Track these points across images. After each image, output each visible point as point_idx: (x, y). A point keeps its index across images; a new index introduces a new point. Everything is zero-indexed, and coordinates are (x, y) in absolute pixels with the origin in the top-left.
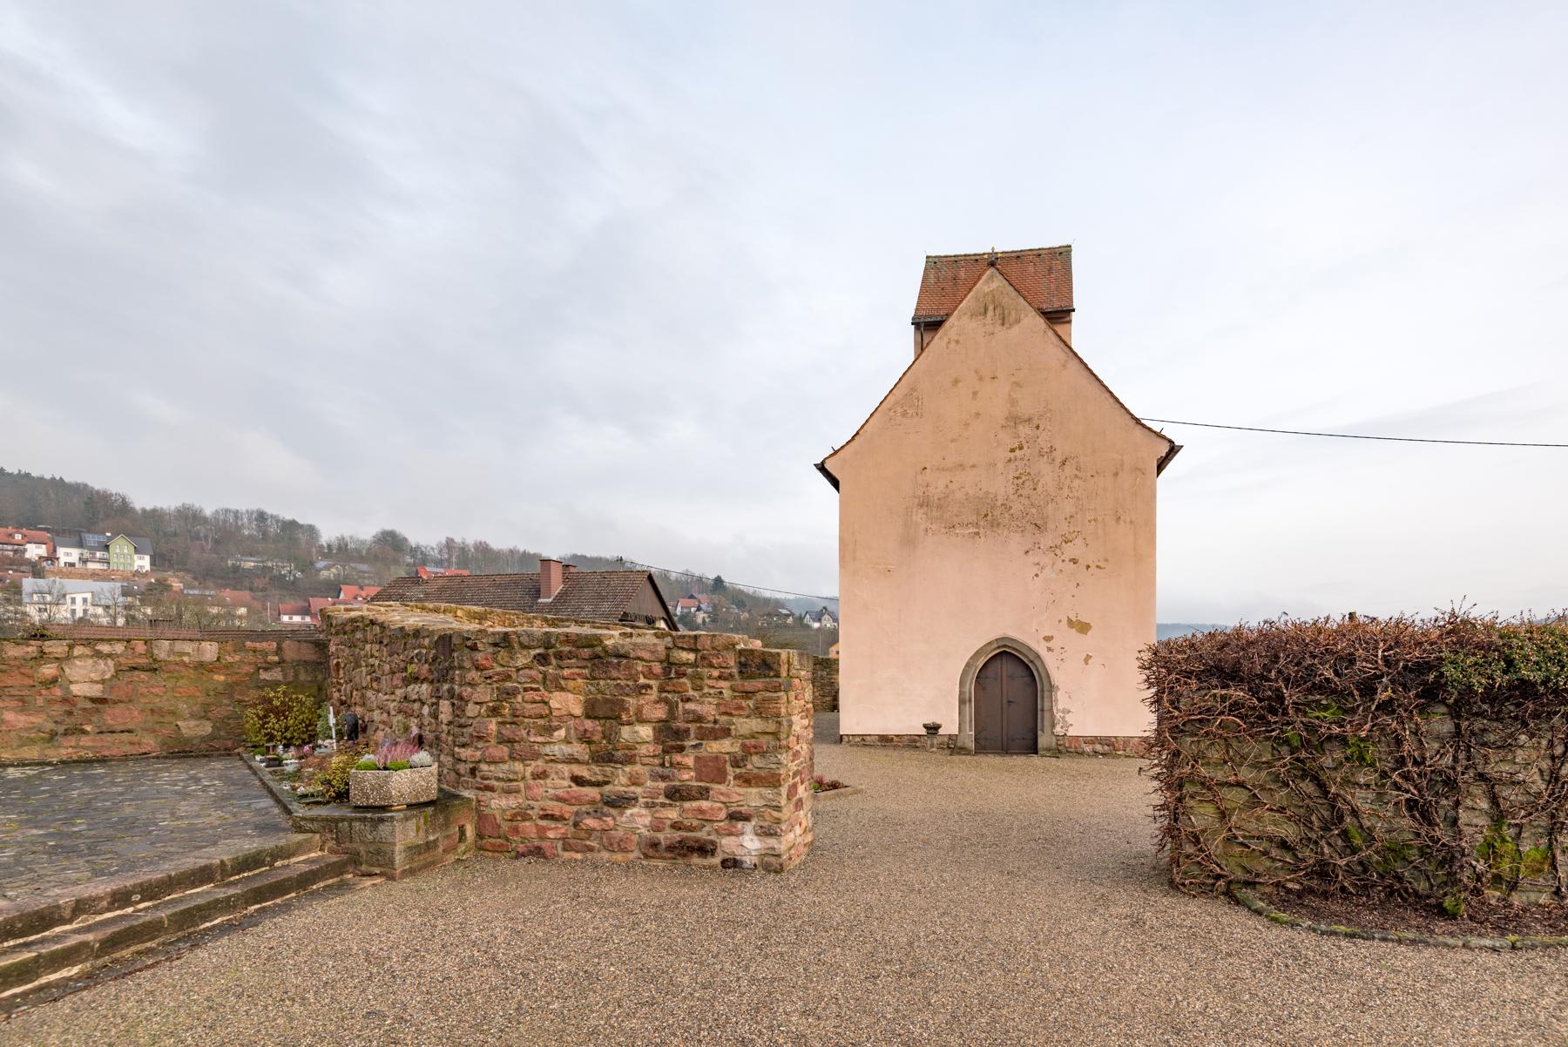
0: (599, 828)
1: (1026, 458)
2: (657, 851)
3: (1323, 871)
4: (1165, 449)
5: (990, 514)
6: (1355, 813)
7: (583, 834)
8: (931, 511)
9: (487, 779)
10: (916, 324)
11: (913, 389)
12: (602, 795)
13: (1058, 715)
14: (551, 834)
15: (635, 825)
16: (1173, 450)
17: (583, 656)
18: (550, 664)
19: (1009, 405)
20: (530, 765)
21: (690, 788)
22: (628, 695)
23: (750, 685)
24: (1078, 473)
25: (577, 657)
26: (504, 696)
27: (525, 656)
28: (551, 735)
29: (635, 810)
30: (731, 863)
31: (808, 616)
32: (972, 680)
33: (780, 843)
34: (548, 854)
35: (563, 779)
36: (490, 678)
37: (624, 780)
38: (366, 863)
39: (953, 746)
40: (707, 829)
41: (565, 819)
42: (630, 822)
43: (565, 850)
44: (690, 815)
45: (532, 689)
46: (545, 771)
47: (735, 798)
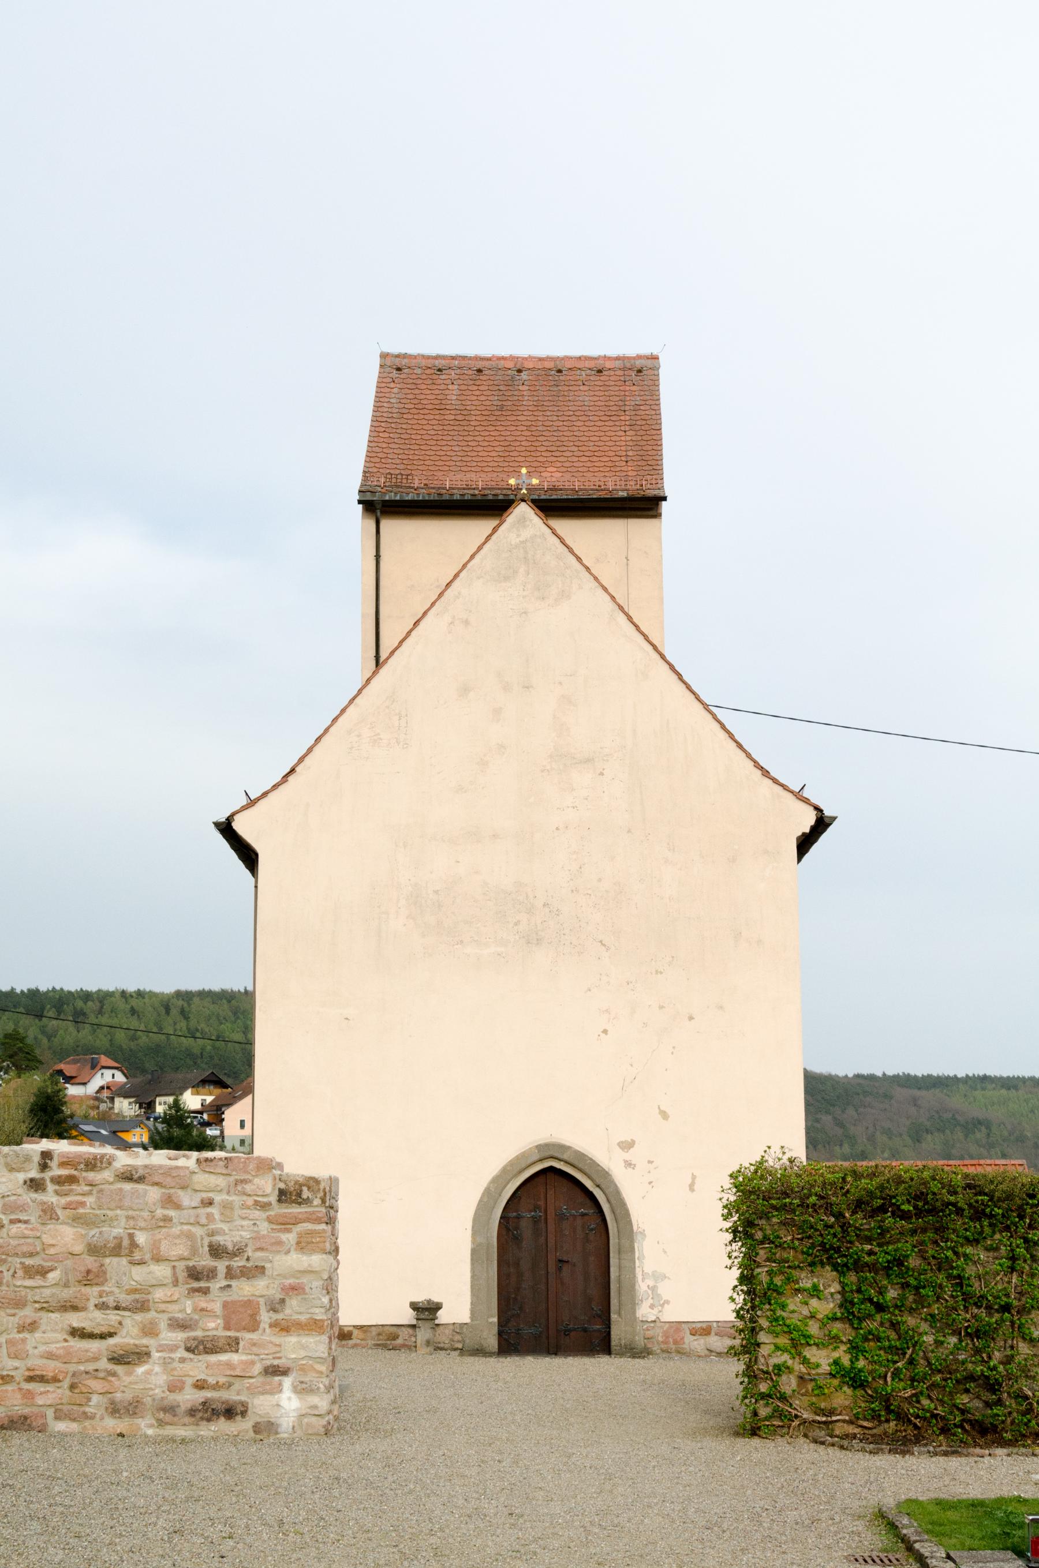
4: (807, 821)
16: (822, 824)
21: (214, 1339)
43: (57, 1418)
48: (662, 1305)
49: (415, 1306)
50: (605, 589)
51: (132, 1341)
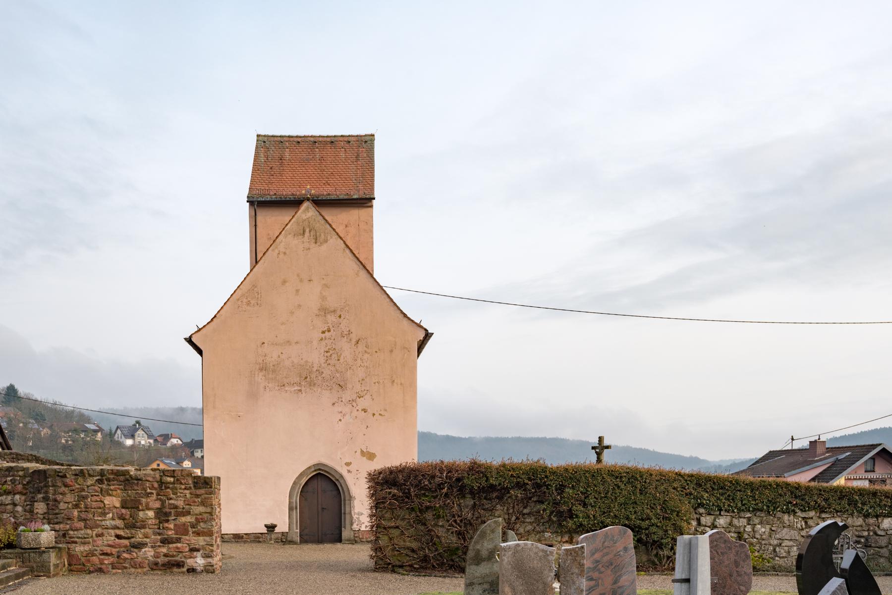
0: (129, 558)
1: (332, 338)
2: (157, 567)
3: (425, 559)
4: (421, 336)
5: (309, 377)
6: (438, 537)
7: (121, 561)
8: (268, 374)
9: (74, 538)
10: (251, 202)
11: (254, 286)
12: (130, 543)
13: (355, 517)
14: (106, 562)
15: (147, 556)
16: (428, 336)
17: (120, 480)
18: (104, 483)
19: (321, 300)
20: (95, 531)
22: (142, 497)
23: (199, 492)
24: (367, 350)
25: (117, 480)
26: (82, 499)
27: (91, 480)
28: (105, 517)
29: (146, 549)
30: (192, 570)
31: (119, 432)
32: (297, 493)
33: (213, 560)
34: (105, 571)
35: (111, 536)
36: (73, 490)
37: (141, 536)
38: (37, 571)
39: (284, 540)
40: (180, 556)
41: (113, 555)
42: (144, 554)
43: (113, 569)
44: (172, 550)
45: (95, 495)
46: (103, 533)
47: (193, 541)
48: (361, 524)
49: (266, 526)
50: (341, 238)
51: (140, 540)
